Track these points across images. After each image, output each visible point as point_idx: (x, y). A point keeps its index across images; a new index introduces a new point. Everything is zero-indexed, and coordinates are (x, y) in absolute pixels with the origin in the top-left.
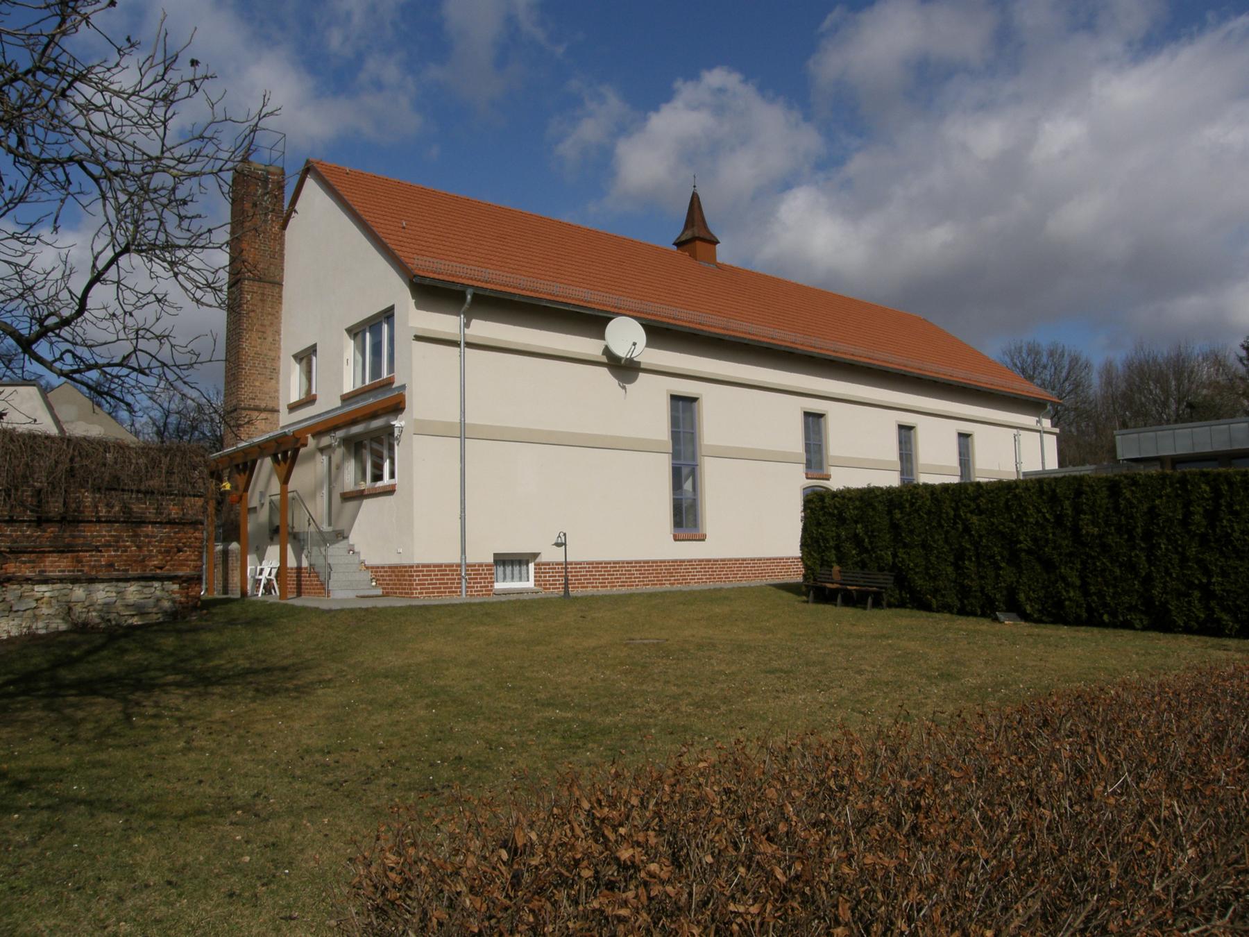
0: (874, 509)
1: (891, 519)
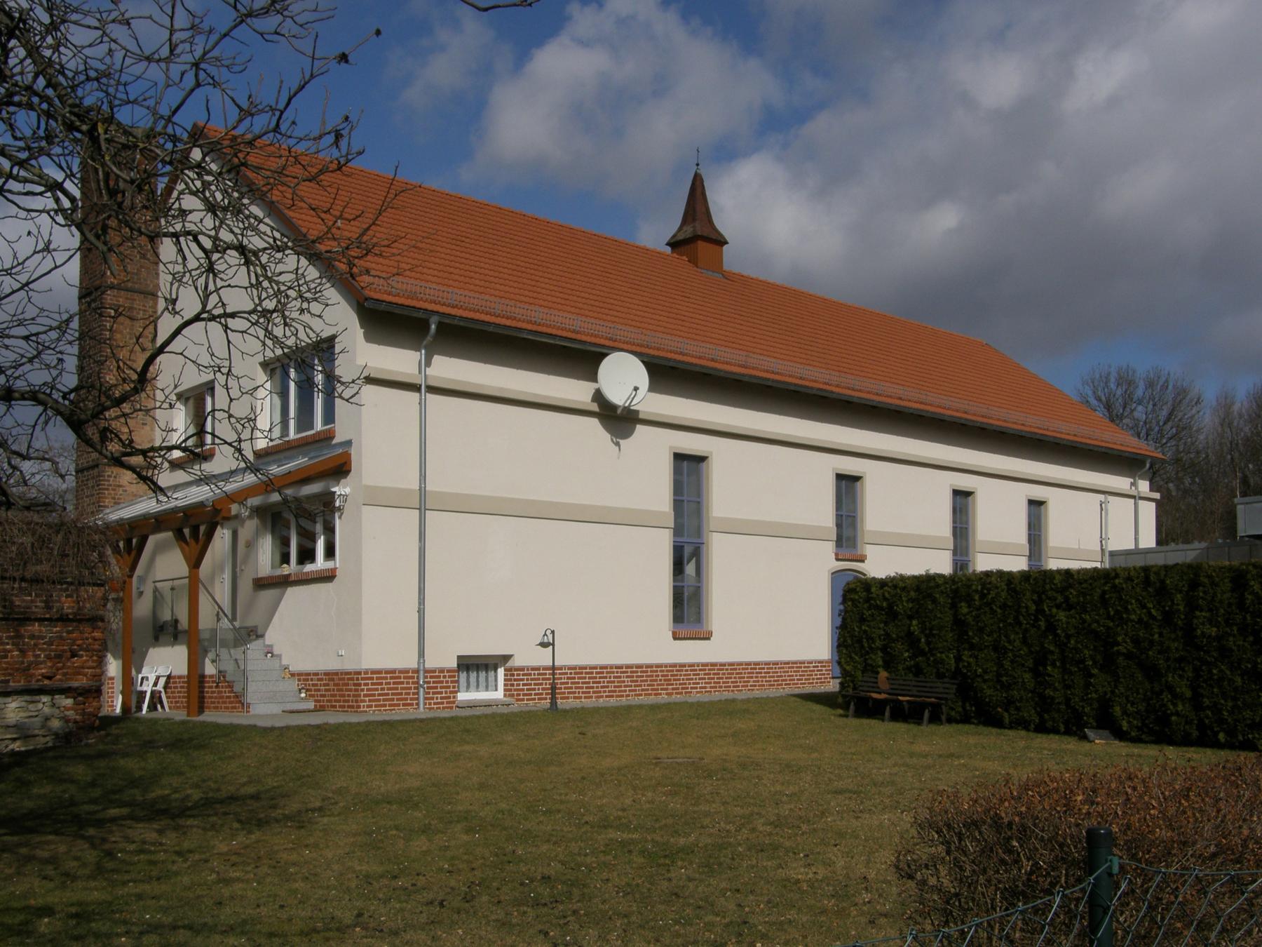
0: (934, 601)
1: (955, 615)
